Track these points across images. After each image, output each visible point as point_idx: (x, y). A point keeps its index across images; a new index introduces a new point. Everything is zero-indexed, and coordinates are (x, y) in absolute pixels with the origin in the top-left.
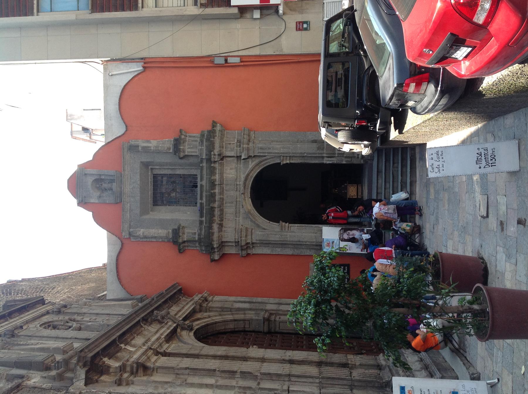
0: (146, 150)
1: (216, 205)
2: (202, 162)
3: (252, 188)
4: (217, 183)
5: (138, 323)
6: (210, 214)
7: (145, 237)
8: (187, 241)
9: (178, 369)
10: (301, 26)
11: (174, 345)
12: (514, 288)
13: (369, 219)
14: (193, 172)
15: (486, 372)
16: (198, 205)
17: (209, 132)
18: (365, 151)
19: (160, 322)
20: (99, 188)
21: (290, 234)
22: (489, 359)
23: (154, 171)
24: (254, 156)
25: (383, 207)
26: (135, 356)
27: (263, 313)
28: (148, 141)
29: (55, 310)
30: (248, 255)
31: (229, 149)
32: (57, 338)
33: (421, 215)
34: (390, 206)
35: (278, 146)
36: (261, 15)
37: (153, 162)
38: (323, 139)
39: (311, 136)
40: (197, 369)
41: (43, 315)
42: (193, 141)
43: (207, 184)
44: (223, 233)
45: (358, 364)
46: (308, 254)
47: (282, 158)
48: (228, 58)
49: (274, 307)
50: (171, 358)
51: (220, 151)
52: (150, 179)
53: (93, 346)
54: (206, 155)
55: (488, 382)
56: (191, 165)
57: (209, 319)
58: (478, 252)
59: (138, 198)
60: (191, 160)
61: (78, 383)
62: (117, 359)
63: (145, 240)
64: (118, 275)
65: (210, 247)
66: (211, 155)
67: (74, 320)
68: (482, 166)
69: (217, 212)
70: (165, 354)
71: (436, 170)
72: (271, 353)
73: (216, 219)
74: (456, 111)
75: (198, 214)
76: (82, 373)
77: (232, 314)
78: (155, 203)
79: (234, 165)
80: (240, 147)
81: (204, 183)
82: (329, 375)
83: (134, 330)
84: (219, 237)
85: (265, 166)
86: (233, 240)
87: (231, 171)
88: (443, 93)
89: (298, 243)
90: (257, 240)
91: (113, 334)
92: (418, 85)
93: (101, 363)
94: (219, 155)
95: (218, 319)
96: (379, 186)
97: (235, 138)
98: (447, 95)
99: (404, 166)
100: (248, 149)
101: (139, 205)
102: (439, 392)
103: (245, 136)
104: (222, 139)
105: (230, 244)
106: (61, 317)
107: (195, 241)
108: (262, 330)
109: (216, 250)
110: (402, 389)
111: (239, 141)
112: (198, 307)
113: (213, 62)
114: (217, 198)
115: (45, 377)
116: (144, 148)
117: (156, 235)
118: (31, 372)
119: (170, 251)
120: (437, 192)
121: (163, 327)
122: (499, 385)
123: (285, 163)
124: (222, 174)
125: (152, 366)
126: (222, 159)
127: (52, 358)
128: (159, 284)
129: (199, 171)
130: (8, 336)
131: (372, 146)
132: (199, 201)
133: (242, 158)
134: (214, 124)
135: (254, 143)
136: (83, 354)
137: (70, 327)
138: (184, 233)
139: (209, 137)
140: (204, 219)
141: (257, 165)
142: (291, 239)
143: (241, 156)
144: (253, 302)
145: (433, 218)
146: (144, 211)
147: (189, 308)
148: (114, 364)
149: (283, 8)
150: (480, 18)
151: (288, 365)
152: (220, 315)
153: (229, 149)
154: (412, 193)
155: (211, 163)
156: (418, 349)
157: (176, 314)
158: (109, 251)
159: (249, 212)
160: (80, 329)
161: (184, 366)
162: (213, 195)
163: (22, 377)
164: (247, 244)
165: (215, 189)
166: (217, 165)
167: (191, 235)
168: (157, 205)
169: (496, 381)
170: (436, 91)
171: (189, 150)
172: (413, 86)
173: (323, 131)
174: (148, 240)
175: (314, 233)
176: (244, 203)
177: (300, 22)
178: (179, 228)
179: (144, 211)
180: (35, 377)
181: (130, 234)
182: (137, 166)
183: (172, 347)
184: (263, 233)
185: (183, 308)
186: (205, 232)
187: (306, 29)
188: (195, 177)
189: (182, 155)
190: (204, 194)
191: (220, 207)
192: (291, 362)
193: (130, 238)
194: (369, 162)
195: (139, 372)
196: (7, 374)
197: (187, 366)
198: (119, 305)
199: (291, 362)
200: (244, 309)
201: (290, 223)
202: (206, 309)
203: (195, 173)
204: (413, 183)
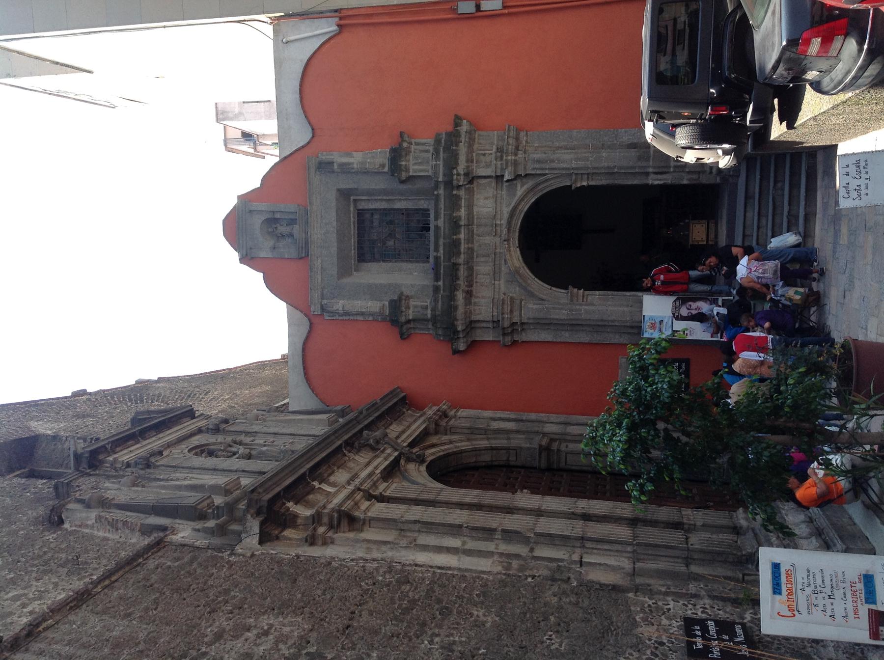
0: (345, 169)
1: (461, 259)
2: (436, 187)
3: (521, 231)
4: (462, 223)
6: (451, 275)
7: (347, 314)
8: (414, 320)
9: (403, 523)
14: (423, 204)
16: (432, 260)
17: (449, 135)
19: (374, 449)
21: (586, 307)
24: (526, 175)
26: (336, 501)
27: (537, 439)
28: (349, 154)
29: (211, 427)
30: (514, 343)
31: (483, 164)
37: (357, 189)
39: (626, 137)
40: (432, 523)
41: (192, 435)
43: (447, 225)
44: (472, 308)
45: (699, 523)
46: (616, 341)
47: (574, 177)
50: (391, 505)
51: (468, 167)
52: (353, 218)
53: (270, 483)
54: (444, 175)
57: (451, 446)
59: (334, 250)
60: (419, 185)
61: (248, 540)
62: (308, 505)
63: (347, 318)
64: (305, 374)
65: (451, 329)
66: (452, 175)
67: (240, 443)
69: (462, 272)
70: (382, 499)
73: (461, 282)
75: (432, 276)
77: (488, 439)
78: (362, 258)
79: (490, 192)
80: (501, 159)
81: (440, 223)
82: (651, 540)
84: (465, 313)
85: (545, 191)
86: (490, 319)
87: (487, 202)
89: (600, 323)
90: (529, 319)
91: (300, 466)
93: (282, 510)
94: (466, 175)
95: (464, 445)
96: (748, 223)
97: (492, 144)
99: (794, 186)
100: (515, 164)
101: (335, 260)
104: (470, 146)
105: (484, 325)
106: (220, 438)
107: (427, 320)
108: (536, 464)
109: (461, 335)
111: (500, 150)
112: (433, 426)
115: (199, 530)
116: (342, 165)
117: (364, 310)
118: (178, 521)
124: (470, 207)
125: (362, 516)
126: (471, 182)
127: (208, 501)
130: (140, 466)
131: (737, 153)
132: (432, 254)
133: (506, 179)
135: (525, 152)
136: (255, 496)
137: (234, 454)
138: (408, 308)
139: (448, 144)
140: (441, 283)
143: (503, 176)
144: (522, 421)
146: (344, 271)
147: (418, 427)
148: (303, 512)
152: (468, 440)
153: (483, 164)
154: (807, 235)
155: (453, 188)
156: (804, 504)
157: (398, 437)
159: (517, 271)
160: (249, 457)
161: (412, 518)
162: (456, 244)
163: (164, 529)
165: (459, 233)
166: (462, 193)
171: (416, 167)
174: (351, 318)
175: (628, 306)
176: (508, 257)
178: (400, 299)
179: (344, 271)
180: (183, 530)
181: (323, 309)
182: (332, 196)
183: (393, 488)
184: (541, 307)
185: (409, 427)
186: (443, 302)
188: (425, 212)
189: (404, 175)
190: (441, 242)
191: (468, 263)
192: (586, 517)
197: (417, 518)
199: (586, 517)
201: (586, 290)
203: (425, 206)
204: (809, 217)
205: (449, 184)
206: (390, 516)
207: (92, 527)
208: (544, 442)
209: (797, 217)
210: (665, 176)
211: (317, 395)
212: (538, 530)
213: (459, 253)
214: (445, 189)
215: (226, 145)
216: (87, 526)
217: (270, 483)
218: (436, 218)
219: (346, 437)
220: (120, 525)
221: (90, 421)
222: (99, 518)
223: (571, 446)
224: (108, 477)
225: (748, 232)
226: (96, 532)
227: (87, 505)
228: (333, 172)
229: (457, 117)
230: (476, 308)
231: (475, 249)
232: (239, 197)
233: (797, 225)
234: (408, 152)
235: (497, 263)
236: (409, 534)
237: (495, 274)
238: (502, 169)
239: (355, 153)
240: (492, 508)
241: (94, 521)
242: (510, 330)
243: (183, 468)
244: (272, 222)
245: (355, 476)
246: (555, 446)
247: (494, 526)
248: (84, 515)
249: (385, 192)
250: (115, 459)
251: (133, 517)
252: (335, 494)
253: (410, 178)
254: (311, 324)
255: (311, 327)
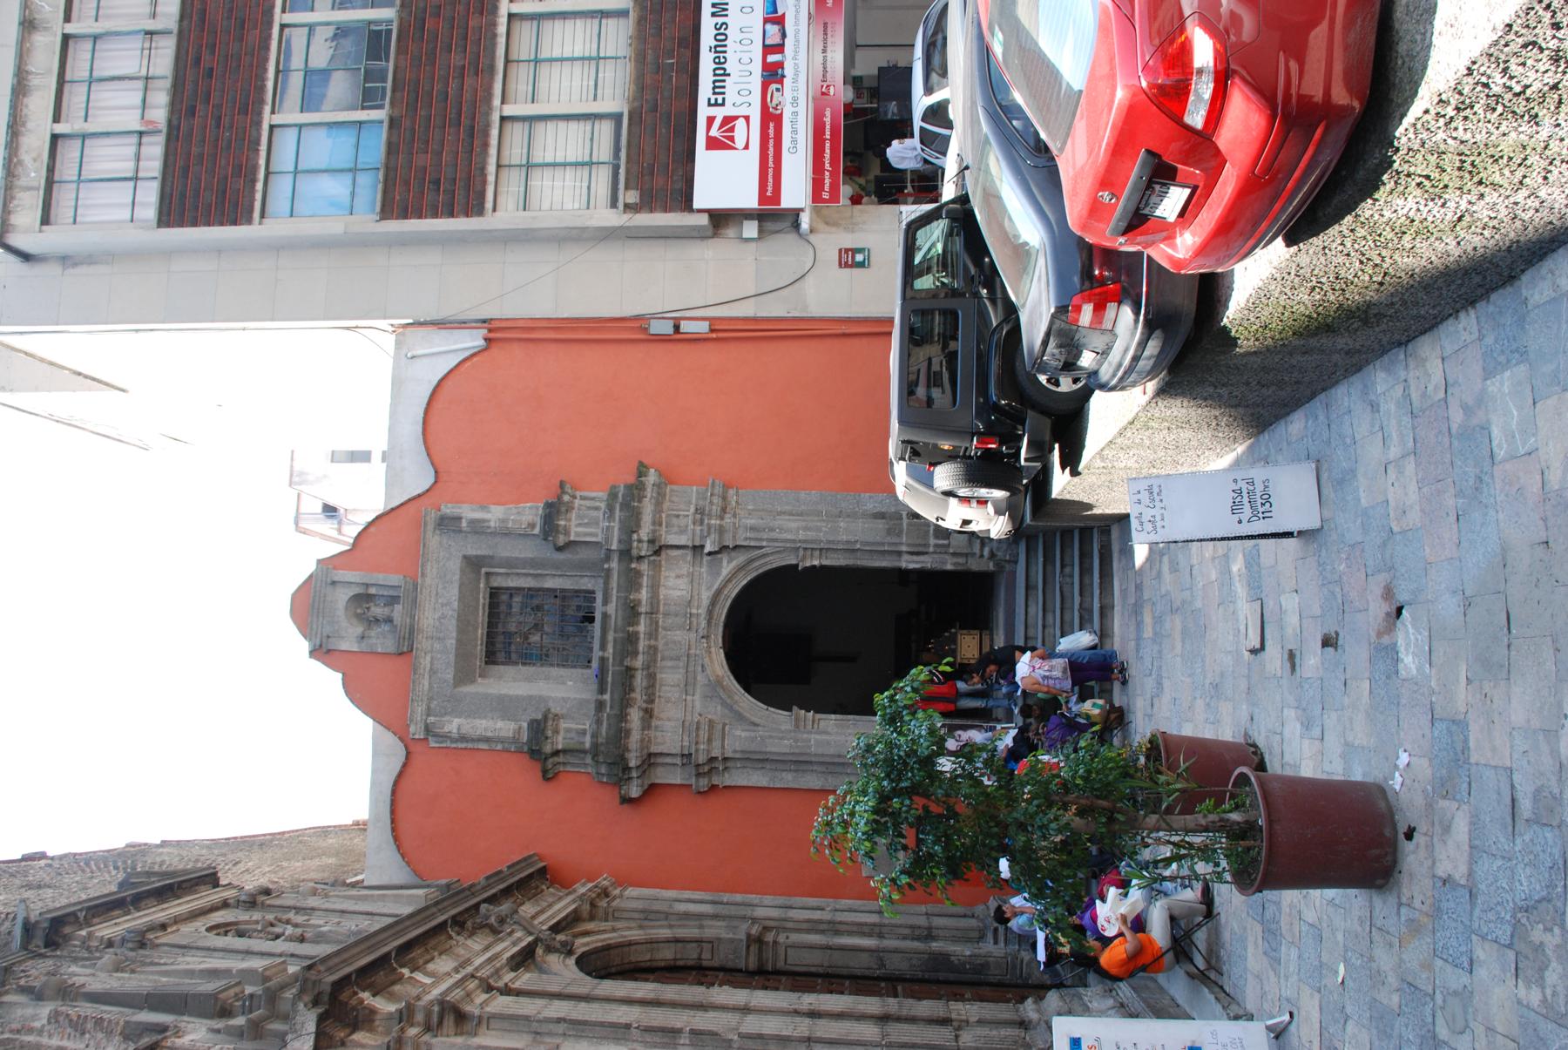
0: (478, 528)
1: (639, 662)
2: (608, 559)
3: (726, 626)
4: (643, 609)
5: (442, 927)
6: (622, 685)
7: (463, 738)
8: (565, 751)
9: (539, 1021)
10: (851, 259)
11: (528, 975)
12: (1319, 776)
13: (1006, 702)
14: (586, 584)
15: (1265, 1006)
16: (595, 664)
17: (629, 487)
18: (997, 526)
19: (495, 931)
20: (359, 617)
22: (1271, 973)
23: (492, 579)
24: (736, 547)
25: (1038, 663)
26: (436, 992)
27: (744, 926)
28: (484, 508)
29: (243, 898)
30: (713, 788)
31: (675, 529)
32: (248, 953)
33: (1124, 682)
34: (1055, 662)
35: (793, 525)
36: (760, 231)
37: (492, 557)
38: (901, 498)
39: (872, 502)
40: (585, 1023)
41: (213, 909)
42: (589, 508)
44: (652, 733)
45: (973, 1019)
47: (801, 552)
48: (683, 323)
49: (775, 913)
50: (521, 999)
51: (654, 531)
52: (483, 599)
53: (336, 960)
54: (620, 541)
55: (1270, 1022)
56: (581, 566)
58: (1246, 734)
59: (451, 643)
60: (583, 554)
61: (296, 1044)
62: (392, 997)
63: (463, 745)
64: (393, 830)
65: (622, 769)
66: (630, 541)
67: (288, 922)
68: (1245, 518)
69: (639, 680)
70: (507, 991)
71: (1149, 527)
72: (762, 998)
73: (638, 696)
74: (1183, 395)
75: (595, 687)
76: (308, 1021)
77: (671, 926)
78: (491, 658)
79: (685, 568)
80: (702, 523)
81: (611, 609)
82: (905, 1039)
83: (433, 942)
84: (642, 740)
86: (677, 750)
87: (679, 581)
88: (1151, 327)
91: (383, 943)
92: (1100, 308)
93: (353, 1002)
94: (651, 542)
95: (635, 934)
96: (1030, 621)
98: (1158, 333)
99: (1085, 571)
100: (721, 530)
101: (452, 657)
102: (1159, 1048)
103: (715, 500)
104: (658, 504)
105: (668, 760)
106: (257, 916)
107: (584, 752)
108: (742, 965)
109: (634, 774)
110: (1076, 1043)
111: (700, 511)
112: (587, 907)
113: (646, 330)
114: (642, 645)
115: (218, 1031)
116: (472, 522)
117: (489, 734)
118: (186, 1018)
119: (523, 775)
120: (1158, 620)
121: (502, 940)
122: (1293, 1027)
123: (808, 564)
124: (655, 588)
125: (477, 1012)
126: (657, 552)
127: (237, 989)
128: (489, 854)
129: (601, 581)
130: (130, 945)
131: (1010, 509)
132: (597, 654)
133: (707, 550)
134: (642, 471)
135: (734, 516)
136: (312, 975)
137: (277, 937)
138: (556, 732)
139: (628, 501)
140: (607, 697)
141: (740, 569)
142: (820, 751)
143: (702, 547)
145: (1150, 683)
146: (464, 675)
147: (565, 907)
148: (384, 1006)
149: (811, 219)
150: (1196, 118)
151: (807, 1021)
152: (641, 927)
153: (675, 529)
154: (1104, 634)
155: (631, 561)
156: (1114, 971)
157: (533, 917)
158: (374, 771)
159: (719, 682)
160: (302, 939)
161: (554, 1015)
162: (632, 639)
163: (162, 1029)
164: (713, 759)
165: (638, 623)
166: (644, 567)
167: (573, 735)
168: (495, 663)
169: (1287, 1017)
170: (1136, 321)
171: (580, 529)
172: (1087, 311)
173: (900, 470)
174: (470, 745)
176: (707, 660)
177: (847, 251)
178: (545, 717)
179: (464, 675)
180: (194, 1030)
181: (427, 729)
182: (455, 565)
183: (525, 979)
185: (550, 906)
186: (609, 725)
187: (861, 265)
188: (589, 595)
189: (561, 540)
190: (611, 636)
191: (648, 667)
192: (814, 1014)
193: (426, 739)
194: (1008, 567)
195: (445, 1023)
196: (127, 1023)
197: (561, 1015)
198: (395, 896)
199: (814, 1014)
200: (700, 916)
201: (817, 712)
202: (606, 914)
203: (590, 587)
204: (1106, 610)
205: (626, 554)
206: (520, 1012)
207: (40, 1032)
208: (755, 931)
209: (1091, 611)
210: (921, 558)
211: (408, 864)
212: (743, 1030)
213: (636, 653)
214: (620, 560)
215: (296, 523)
216: (31, 1031)
217: (336, 960)
218: (605, 603)
219: (454, 912)
220: (89, 1026)
221: (49, 893)
222: (55, 1017)
223: (795, 938)
224: (75, 960)
225: (1031, 633)
226: (45, 1040)
227: (37, 995)
228: (461, 531)
229: (641, 464)
230: (659, 734)
231: (660, 647)
232: (319, 562)
233: (1091, 621)
234: (570, 508)
235: (691, 669)
236: (548, 1040)
237: (688, 685)
238: (703, 537)
239: (493, 508)
240: (674, 1005)
241: (45, 1021)
242: (706, 769)
243: (197, 948)
244: (362, 599)
245: (468, 962)
246: (769, 937)
247: (679, 1025)
248: (29, 1011)
249: (533, 563)
250: (90, 934)
251: (110, 1012)
252: (433, 985)
253: (570, 545)
254: (408, 754)
255: (407, 757)
